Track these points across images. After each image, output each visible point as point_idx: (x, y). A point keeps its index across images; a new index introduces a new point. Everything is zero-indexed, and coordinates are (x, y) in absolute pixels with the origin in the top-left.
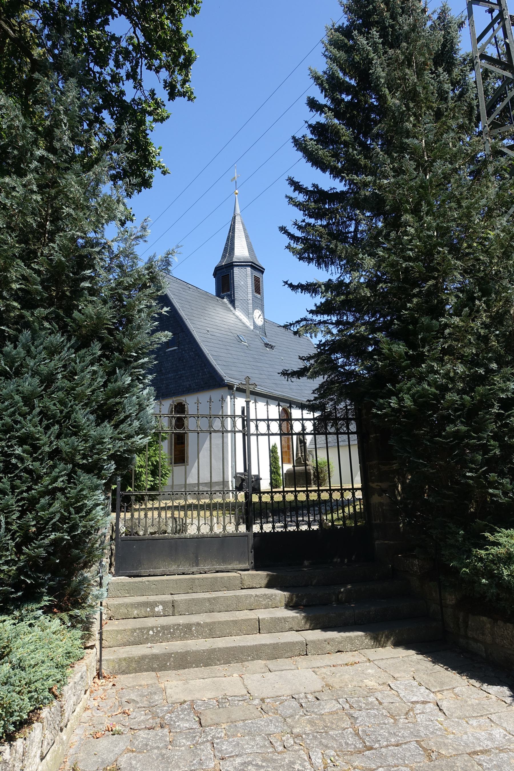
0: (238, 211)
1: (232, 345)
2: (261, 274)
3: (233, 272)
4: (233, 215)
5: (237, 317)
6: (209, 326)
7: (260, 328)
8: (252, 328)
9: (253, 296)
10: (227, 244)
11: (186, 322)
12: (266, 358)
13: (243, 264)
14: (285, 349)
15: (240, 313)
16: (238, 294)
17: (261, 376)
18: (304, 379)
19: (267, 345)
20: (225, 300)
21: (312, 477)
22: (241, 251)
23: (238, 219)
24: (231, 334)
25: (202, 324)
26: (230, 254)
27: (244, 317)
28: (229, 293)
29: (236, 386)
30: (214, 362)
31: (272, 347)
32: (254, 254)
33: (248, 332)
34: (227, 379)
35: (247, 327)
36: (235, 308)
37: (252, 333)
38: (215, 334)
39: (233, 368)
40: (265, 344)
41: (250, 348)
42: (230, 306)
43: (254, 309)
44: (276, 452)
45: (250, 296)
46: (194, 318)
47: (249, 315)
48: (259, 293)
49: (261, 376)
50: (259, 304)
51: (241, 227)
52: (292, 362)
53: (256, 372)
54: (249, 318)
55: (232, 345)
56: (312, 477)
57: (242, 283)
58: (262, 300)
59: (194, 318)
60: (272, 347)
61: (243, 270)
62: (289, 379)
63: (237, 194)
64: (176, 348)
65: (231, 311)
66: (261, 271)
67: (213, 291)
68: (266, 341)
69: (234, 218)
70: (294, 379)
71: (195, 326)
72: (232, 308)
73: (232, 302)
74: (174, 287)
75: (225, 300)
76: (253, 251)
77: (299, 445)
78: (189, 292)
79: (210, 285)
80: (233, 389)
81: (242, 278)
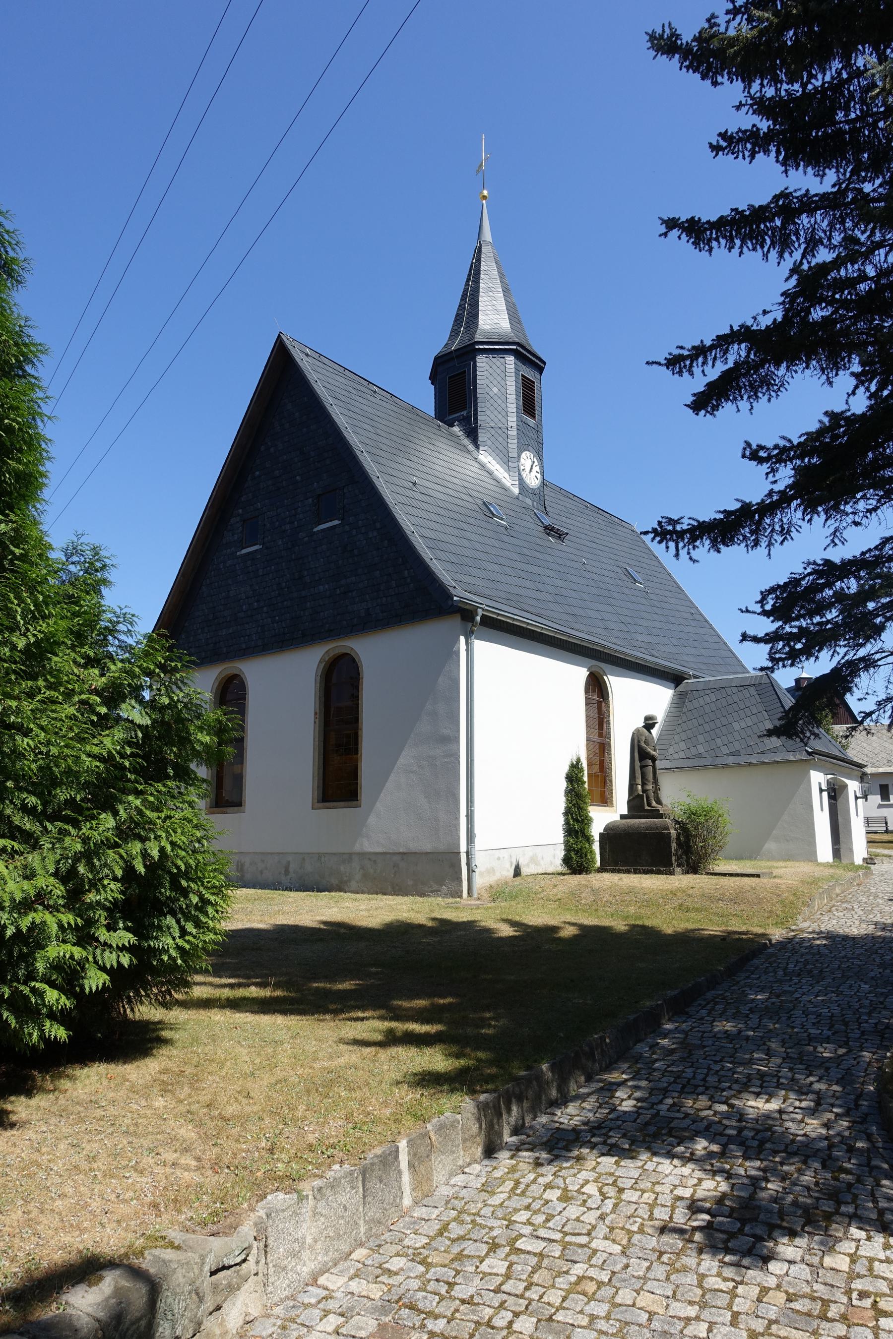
0: (487, 236)
1: (472, 521)
2: (538, 376)
3: (475, 366)
4: (475, 244)
5: (483, 466)
6: (417, 473)
7: (533, 492)
8: (516, 491)
9: (520, 420)
10: (461, 307)
11: (361, 458)
12: (549, 558)
13: (499, 348)
14: (589, 544)
15: (490, 459)
16: (486, 416)
17: (539, 595)
18: (735, 552)
19: (549, 530)
20: (456, 429)
21: (674, 846)
22: (493, 318)
23: (488, 268)
24: (470, 499)
25: (401, 468)
26: (467, 327)
27: (498, 467)
28: (464, 413)
29: (480, 612)
30: (426, 554)
31: (560, 536)
32: (523, 330)
33: (506, 498)
34: (459, 593)
35: (505, 489)
36: (477, 447)
37: (516, 502)
38: (431, 492)
39: (472, 571)
40: (546, 528)
41: (512, 533)
42: (466, 442)
43: (520, 451)
44: (580, 781)
45: (512, 420)
46: (382, 453)
47: (509, 462)
48: (533, 416)
49: (539, 595)
50: (533, 440)
51: (494, 268)
52: (606, 573)
53: (528, 584)
54: (509, 469)
55: (472, 521)
56: (674, 846)
57: (495, 390)
58: (539, 431)
59: (382, 453)
60: (560, 536)
61: (497, 361)
62: (683, 553)
63: (484, 197)
64: (336, 522)
65: (469, 452)
66: (538, 365)
67: (428, 405)
68: (547, 521)
69: (479, 251)
70: (703, 549)
71: (382, 468)
72: (471, 447)
73: (472, 434)
74: (337, 384)
75: (456, 429)
76: (520, 323)
77: (638, 764)
78: (372, 399)
79: (424, 397)
80: (472, 619)
81: (497, 380)
